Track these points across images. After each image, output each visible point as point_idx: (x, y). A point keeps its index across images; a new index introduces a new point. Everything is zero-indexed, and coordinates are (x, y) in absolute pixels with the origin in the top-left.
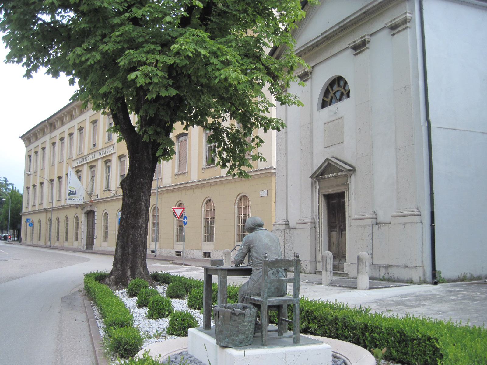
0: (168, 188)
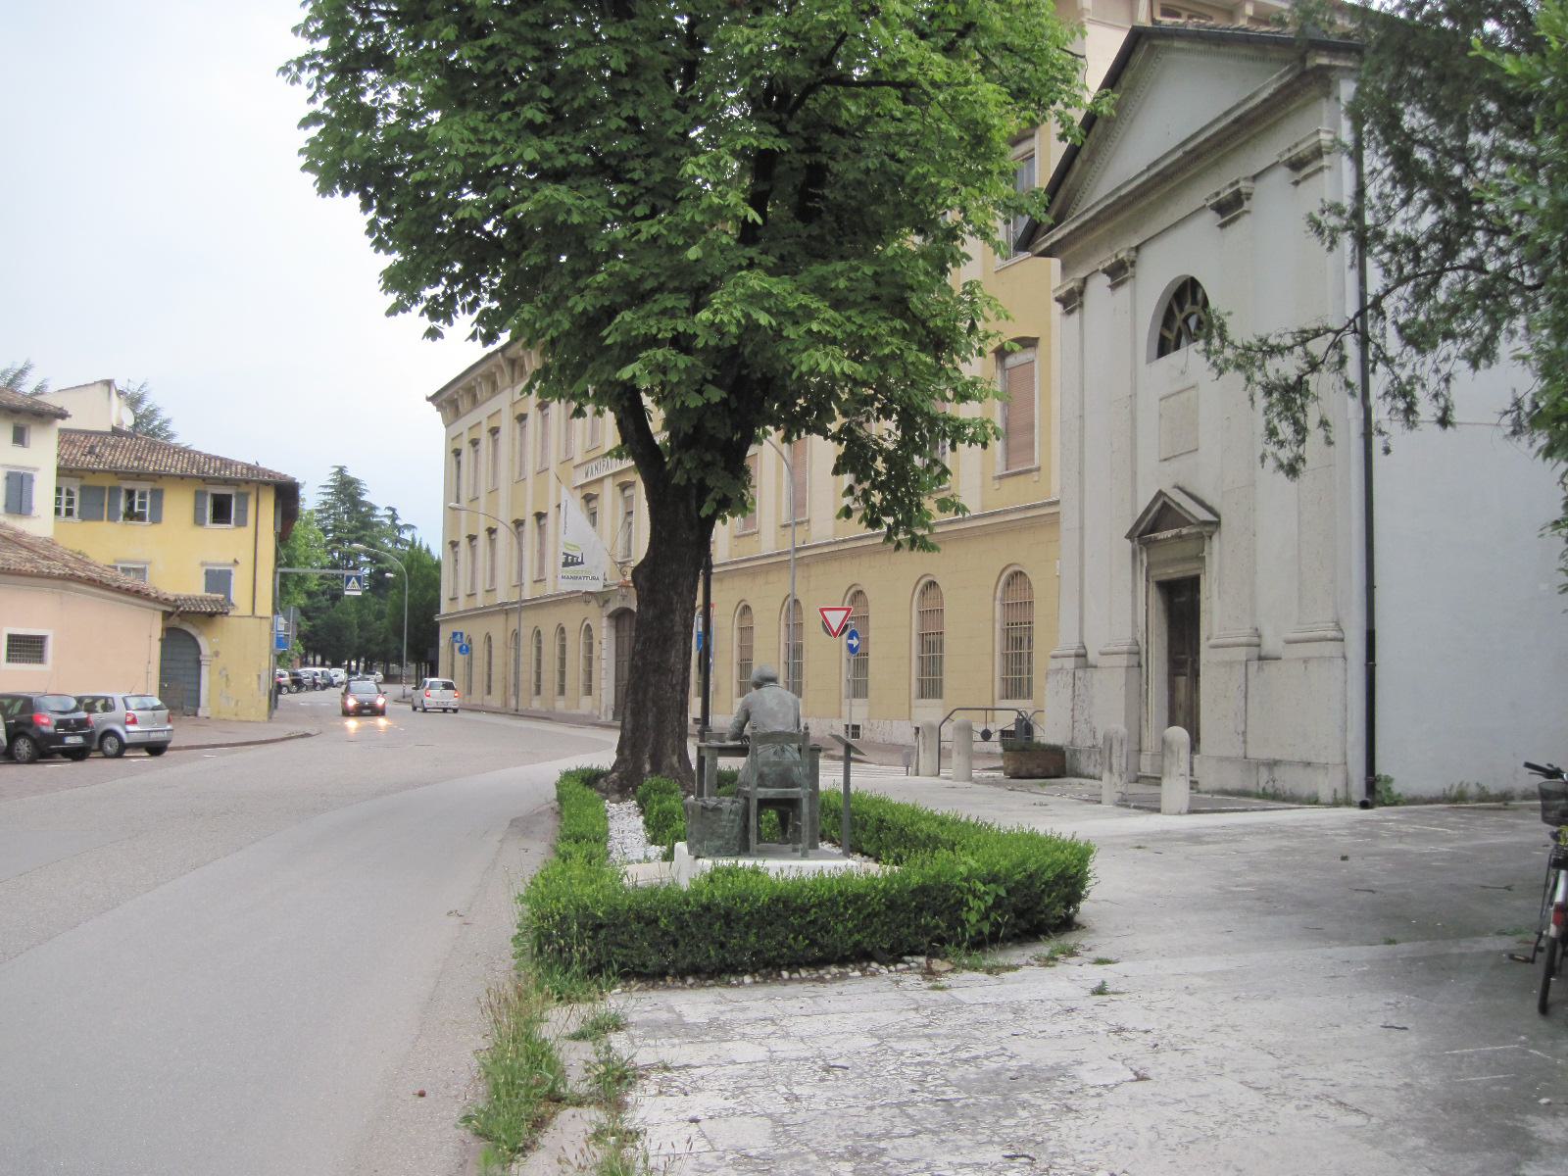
0: (826, 550)
